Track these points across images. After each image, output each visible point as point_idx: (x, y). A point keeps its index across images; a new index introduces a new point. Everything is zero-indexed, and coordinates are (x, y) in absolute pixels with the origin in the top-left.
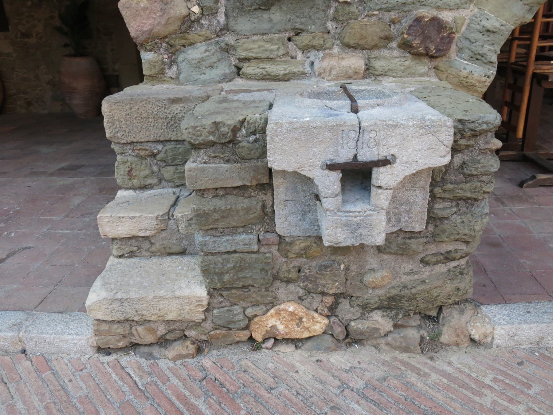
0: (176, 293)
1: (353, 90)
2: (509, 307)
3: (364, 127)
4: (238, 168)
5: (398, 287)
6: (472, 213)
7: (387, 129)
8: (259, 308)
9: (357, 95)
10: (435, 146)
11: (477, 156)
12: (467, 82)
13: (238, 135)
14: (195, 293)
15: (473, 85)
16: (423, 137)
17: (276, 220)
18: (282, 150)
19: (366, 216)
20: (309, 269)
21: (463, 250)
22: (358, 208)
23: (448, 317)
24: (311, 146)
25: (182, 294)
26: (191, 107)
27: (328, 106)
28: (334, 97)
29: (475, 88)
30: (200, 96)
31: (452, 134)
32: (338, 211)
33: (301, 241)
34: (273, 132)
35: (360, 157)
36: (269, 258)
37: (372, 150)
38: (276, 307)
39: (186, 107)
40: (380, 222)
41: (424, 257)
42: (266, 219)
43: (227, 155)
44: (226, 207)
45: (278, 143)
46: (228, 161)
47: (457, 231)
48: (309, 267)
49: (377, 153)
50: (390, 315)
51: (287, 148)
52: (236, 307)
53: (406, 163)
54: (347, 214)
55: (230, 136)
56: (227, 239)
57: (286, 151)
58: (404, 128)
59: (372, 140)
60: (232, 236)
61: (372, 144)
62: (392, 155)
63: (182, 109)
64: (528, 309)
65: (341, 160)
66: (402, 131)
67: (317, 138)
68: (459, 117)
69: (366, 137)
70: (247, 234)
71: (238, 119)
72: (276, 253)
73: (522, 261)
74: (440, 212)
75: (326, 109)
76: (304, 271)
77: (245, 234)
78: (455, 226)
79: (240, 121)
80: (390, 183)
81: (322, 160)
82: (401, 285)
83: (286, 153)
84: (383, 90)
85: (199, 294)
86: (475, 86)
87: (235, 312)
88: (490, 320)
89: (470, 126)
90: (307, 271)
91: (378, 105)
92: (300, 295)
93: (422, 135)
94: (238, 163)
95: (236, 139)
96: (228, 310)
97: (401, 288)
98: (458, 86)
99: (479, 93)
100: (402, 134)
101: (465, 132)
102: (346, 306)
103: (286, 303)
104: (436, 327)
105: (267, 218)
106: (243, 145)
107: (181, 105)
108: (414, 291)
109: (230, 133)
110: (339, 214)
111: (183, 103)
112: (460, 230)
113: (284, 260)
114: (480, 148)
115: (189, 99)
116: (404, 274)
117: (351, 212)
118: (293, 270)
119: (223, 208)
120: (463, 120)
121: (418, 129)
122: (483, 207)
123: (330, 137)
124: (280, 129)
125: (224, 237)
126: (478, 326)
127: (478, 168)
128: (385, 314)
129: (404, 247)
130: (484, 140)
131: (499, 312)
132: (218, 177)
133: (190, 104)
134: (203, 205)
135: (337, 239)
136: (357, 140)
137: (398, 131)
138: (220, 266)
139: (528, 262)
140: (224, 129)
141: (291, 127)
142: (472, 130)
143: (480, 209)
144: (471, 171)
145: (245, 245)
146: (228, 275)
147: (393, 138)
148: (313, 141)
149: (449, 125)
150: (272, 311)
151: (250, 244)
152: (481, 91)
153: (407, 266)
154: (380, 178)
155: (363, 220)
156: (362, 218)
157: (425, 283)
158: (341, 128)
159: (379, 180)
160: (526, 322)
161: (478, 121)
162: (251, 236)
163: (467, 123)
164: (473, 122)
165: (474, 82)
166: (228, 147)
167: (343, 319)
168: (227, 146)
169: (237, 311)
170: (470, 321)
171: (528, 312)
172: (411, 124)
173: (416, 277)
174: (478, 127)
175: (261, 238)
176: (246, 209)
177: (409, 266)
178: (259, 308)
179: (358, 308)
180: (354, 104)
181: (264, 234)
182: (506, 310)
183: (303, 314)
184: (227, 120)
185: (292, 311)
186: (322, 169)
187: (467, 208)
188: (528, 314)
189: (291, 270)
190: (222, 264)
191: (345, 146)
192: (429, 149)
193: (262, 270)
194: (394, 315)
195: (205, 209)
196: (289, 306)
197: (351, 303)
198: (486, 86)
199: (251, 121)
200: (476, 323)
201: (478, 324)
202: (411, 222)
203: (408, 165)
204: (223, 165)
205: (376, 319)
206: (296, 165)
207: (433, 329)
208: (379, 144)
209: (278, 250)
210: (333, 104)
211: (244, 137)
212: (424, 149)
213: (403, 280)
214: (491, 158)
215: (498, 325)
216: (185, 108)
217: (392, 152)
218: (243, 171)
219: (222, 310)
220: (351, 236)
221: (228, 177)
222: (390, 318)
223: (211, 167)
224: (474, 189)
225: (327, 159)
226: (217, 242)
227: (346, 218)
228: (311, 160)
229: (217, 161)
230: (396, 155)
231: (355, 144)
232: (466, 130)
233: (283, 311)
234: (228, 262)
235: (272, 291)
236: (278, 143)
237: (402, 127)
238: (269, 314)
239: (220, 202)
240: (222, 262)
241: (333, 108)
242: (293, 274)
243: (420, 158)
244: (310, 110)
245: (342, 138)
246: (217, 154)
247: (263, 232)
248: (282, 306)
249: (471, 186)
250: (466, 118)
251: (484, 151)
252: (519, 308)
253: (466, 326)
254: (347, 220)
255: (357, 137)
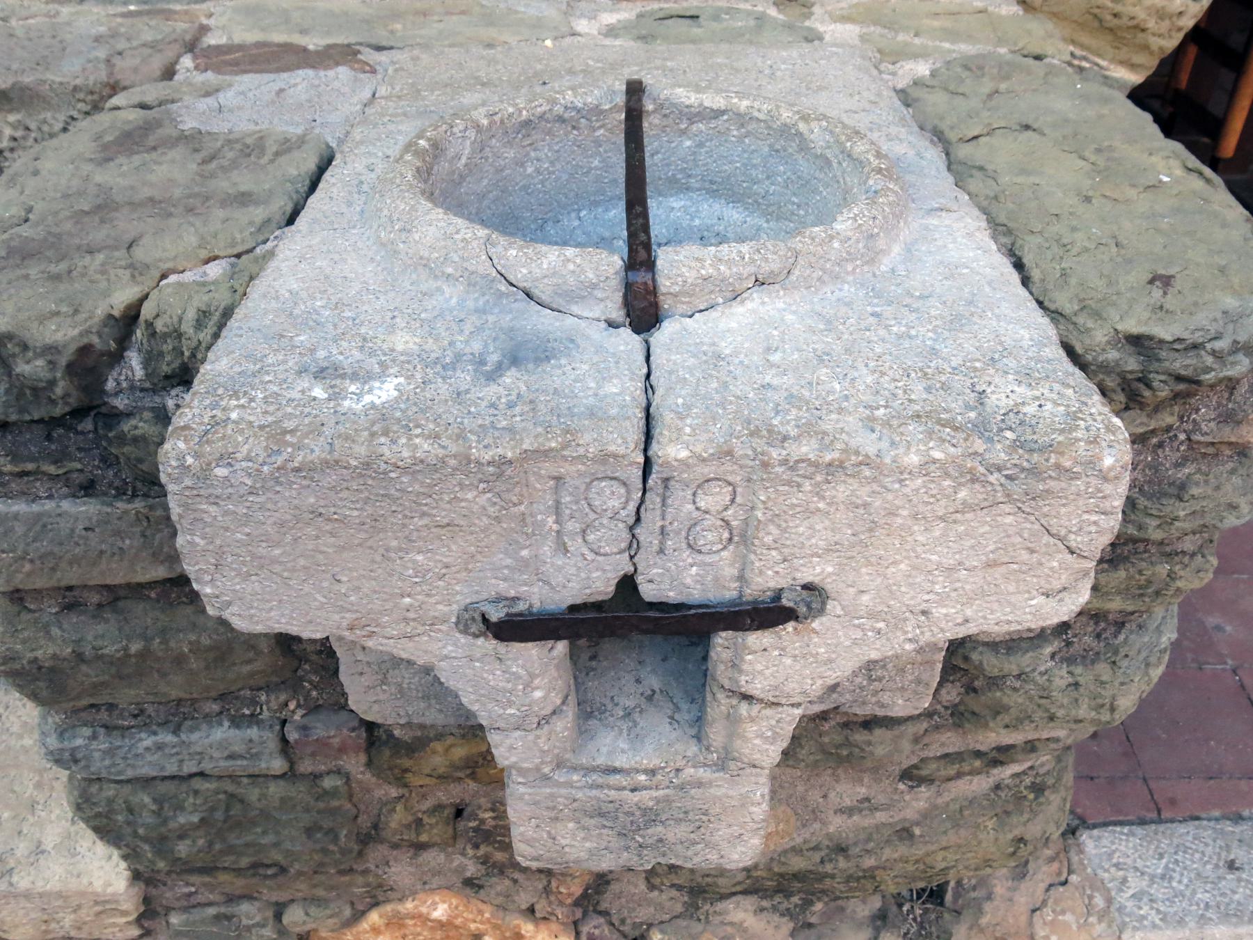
0: (15, 879)
1: (674, 105)
2: (1172, 835)
3: (667, 464)
4: (138, 519)
5: (816, 848)
6: (1116, 652)
7: (789, 483)
8: (328, 912)
9: (694, 128)
10: (1025, 556)
11: (1177, 465)
12: (1115, 15)
13: (110, 385)
14: (85, 881)
15: (1136, 27)
16: (969, 516)
17: (343, 677)
18: (254, 556)
19: (681, 787)
20: (493, 810)
21: (1057, 740)
22: (648, 757)
23: (974, 888)
24: (394, 543)
25: (40, 883)
26: (51, 125)
27: (511, 278)
28: (598, 133)
29: (1140, 35)
30: (78, 82)
31: (1118, 503)
32: (559, 765)
33: (450, 740)
34: (188, 482)
35: (651, 586)
36: (334, 793)
37: (708, 559)
38: (389, 908)
39: (33, 126)
40: (743, 805)
41: (915, 767)
42: (304, 670)
43: (79, 466)
44: (126, 649)
45: (227, 529)
46: (88, 489)
47: (1047, 710)
48: (494, 804)
49: (736, 572)
50: (785, 905)
51: (277, 552)
52: (245, 907)
53: (872, 615)
54: (595, 777)
55: (66, 395)
56: (155, 743)
57: (274, 561)
58: (875, 479)
59: (710, 521)
60: (176, 731)
61: (709, 537)
62: (808, 587)
63: (19, 134)
64: (1228, 848)
65: (557, 597)
66: (863, 493)
67: (424, 514)
68: (1132, 326)
69: (682, 506)
70: (236, 722)
71: (100, 312)
72: (362, 773)
73: (1211, 621)
74: (994, 661)
75: (501, 295)
76: (474, 816)
77: (226, 724)
78: (1042, 697)
79: (111, 316)
80: (792, 686)
81: (463, 600)
82: (827, 843)
83: (277, 568)
84: (802, 126)
85: (98, 886)
86: (1143, 30)
87: (245, 922)
88: (1109, 901)
89: (1177, 364)
90: (488, 815)
91: (759, 283)
92: (468, 874)
93: (967, 507)
94: (134, 496)
95: (105, 404)
96: (218, 918)
97: (823, 853)
98: (1082, 26)
99: (1152, 53)
100: (866, 505)
101: (1149, 386)
102: (636, 886)
103: (421, 896)
104: (933, 916)
105: (307, 667)
106: (137, 432)
107: (12, 118)
108: (869, 862)
109: (61, 384)
110: (561, 777)
111: (18, 110)
112: (1062, 706)
113: (394, 792)
114: (1197, 437)
115: (38, 96)
116: (841, 811)
117: (615, 771)
118: (433, 821)
119: (110, 650)
120: (1150, 338)
121: (947, 483)
122: (1157, 627)
123: (492, 510)
124: (221, 472)
125: (143, 735)
126: (1067, 925)
127: (1176, 519)
128: (765, 903)
129: (845, 753)
130: (1219, 404)
131: (1139, 864)
132: (56, 550)
133: (49, 115)
134: (24, 642)
135: (558, 852)
136: (631, 521)
137: (841, 491)
138: (148, 819)
139: (1229, 628)
140: (30, 368)
141: (280, 460)
142: (1179, 378)
143: (1146, 639)
144: (1140, 528)
145: (231, 757)
146: (188, 842)
147: (816, 519)
148: (404, 526)
149: (1111, 469)
150: (374, 917)
151: (256, 757)
152: (1161, 49)
153: (847, 791)
154: (745, 667)
155: (667, 800)
156: (661, 793)
157: (911, 836)
158: (548, 468)
159: (741, 671)
160: (1226, 917)
161: (1218, 345)
162: (253, 732)
163: (1163, 354)
164: (1195, 346)
165: (1141, 14)
166: (77, 433)
167: (623, 921)
168: (70, 428)
169: (248, 918)
170: (1044, 903)
171: (1231, 866)
172: (914, 459)
173: (881, 817)
174: (1208, 370)
175: (292, 736)
176: (210, 649)
177: (858, 789)
178: (328, 912)
179: (674, 893)
180: (641, 277)
181: (305, 720)
182: (1161, 856)
183: (481, 926)
184: (42, 319)
185: (444, 919)
186: (465, 631)
187: (1098, 636)
188: (1230, 877)
189: (426, 820)
190: (158, 813)
191: (575, 544)
192: (991, 565)
193: (309, 831)
194: (796, 906)
195: (39, 654)
196: (435, 904)
197: (652, 880)
198: (1180, 29)
199: (159, 326)
200: (1063, 912)
201: (1068, 917)
202: (876, 693)
203: (881, 625)
204: (66, 505)
205: (735, 920)
206: (337, 617)
207: (921, 926)
208: (743, 535)
209: (369, 764)
210: (537, 272)
211: (142, 390)
212: (967, 564)
213: (831, 829)
214: (1233, 472)
215: (1135, 929)
216: (27, 129)
217: (807, 576)
218: (160, 531)
219: (197, 915)
220: (616, 843)
221: (102, 552)
222: (782, 915)
223: (16, 517)
224: (1140, 587)
225: (485, 596)
226: (121, 753)
227: (594, 792)
228: (407, 600)
229: (40, 488)
230: (828, 587)
231: (626, 535)
232: (1156, 380)
233: (413, 918)
234: (180, 808)
235: (366, 872)
236: (227, 529)
237: (867, 472)
238: (365, 925)
239: (100, 628)
240: (154, 807)
241: (536, 292)
242: (435, 831)
243: (943, 600)
244: (433, 284)
245: (557, 509)
246: (30, 466)
247: (300, 712)
248: (409, 905)
249: (1130, 578)
250: (1164, 332)
251: (1211, 450)
252: (1201, 847)
253: (1030, 924)
254: (598, 799)
255: (632, 507)
